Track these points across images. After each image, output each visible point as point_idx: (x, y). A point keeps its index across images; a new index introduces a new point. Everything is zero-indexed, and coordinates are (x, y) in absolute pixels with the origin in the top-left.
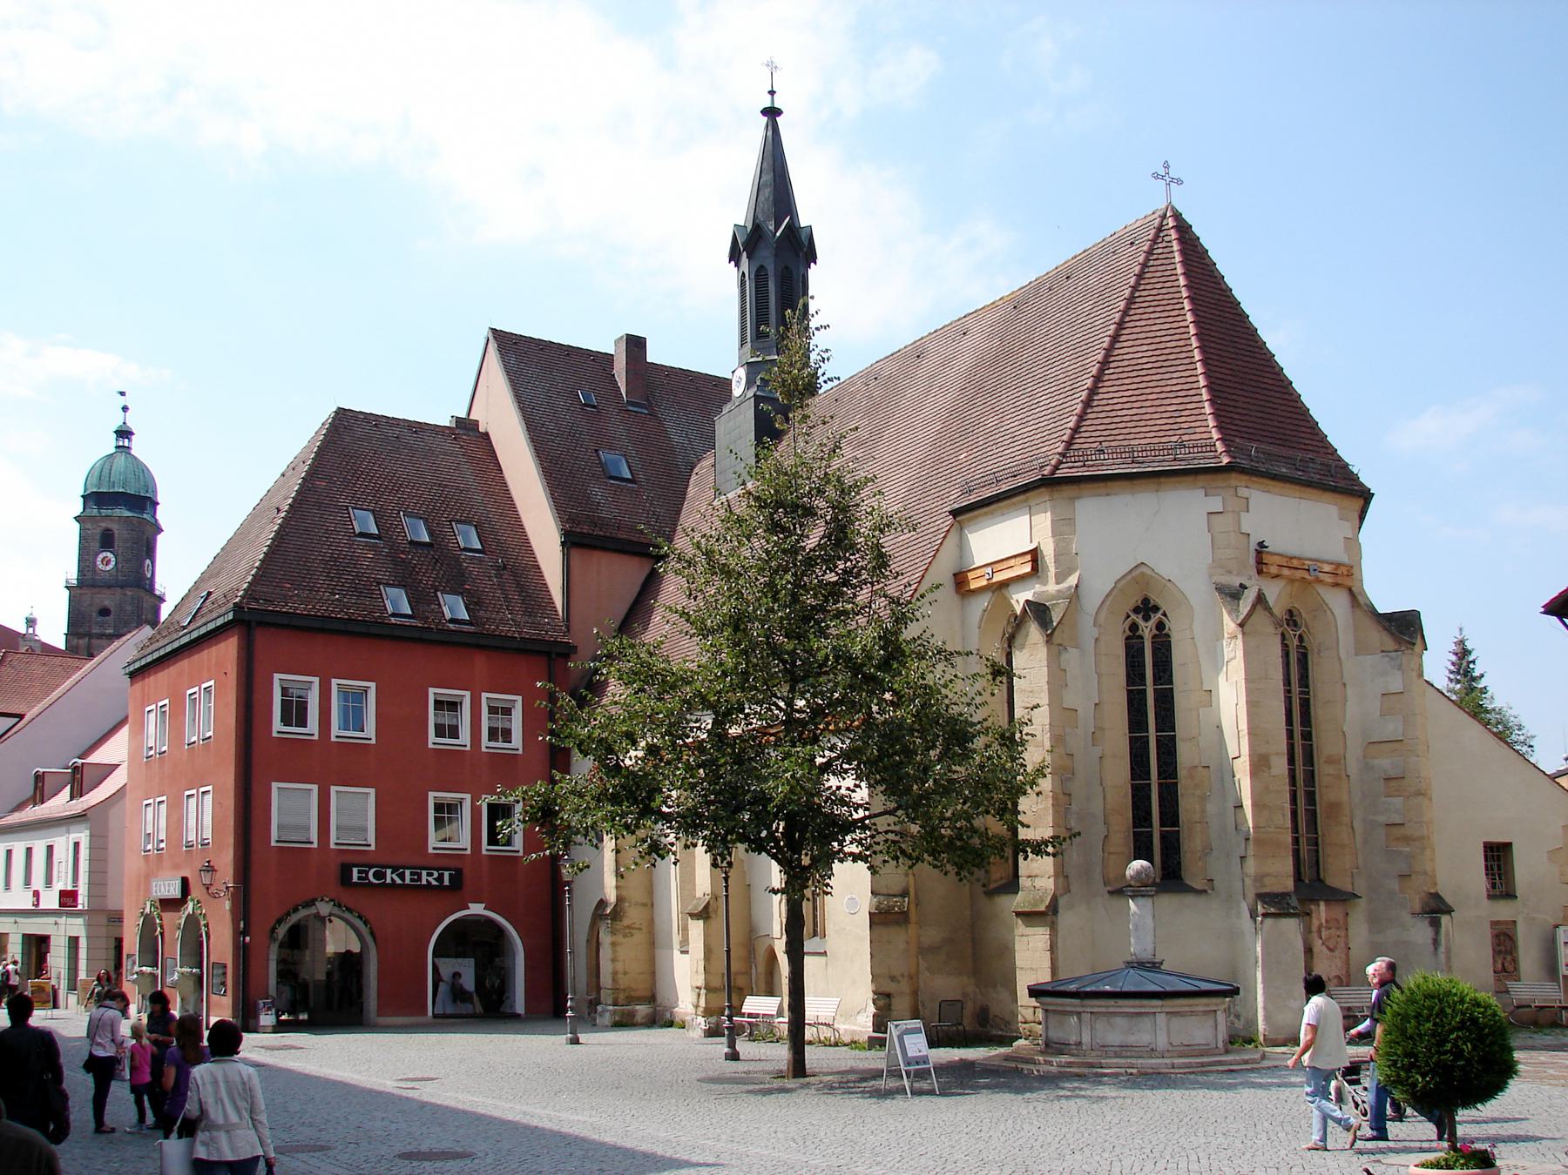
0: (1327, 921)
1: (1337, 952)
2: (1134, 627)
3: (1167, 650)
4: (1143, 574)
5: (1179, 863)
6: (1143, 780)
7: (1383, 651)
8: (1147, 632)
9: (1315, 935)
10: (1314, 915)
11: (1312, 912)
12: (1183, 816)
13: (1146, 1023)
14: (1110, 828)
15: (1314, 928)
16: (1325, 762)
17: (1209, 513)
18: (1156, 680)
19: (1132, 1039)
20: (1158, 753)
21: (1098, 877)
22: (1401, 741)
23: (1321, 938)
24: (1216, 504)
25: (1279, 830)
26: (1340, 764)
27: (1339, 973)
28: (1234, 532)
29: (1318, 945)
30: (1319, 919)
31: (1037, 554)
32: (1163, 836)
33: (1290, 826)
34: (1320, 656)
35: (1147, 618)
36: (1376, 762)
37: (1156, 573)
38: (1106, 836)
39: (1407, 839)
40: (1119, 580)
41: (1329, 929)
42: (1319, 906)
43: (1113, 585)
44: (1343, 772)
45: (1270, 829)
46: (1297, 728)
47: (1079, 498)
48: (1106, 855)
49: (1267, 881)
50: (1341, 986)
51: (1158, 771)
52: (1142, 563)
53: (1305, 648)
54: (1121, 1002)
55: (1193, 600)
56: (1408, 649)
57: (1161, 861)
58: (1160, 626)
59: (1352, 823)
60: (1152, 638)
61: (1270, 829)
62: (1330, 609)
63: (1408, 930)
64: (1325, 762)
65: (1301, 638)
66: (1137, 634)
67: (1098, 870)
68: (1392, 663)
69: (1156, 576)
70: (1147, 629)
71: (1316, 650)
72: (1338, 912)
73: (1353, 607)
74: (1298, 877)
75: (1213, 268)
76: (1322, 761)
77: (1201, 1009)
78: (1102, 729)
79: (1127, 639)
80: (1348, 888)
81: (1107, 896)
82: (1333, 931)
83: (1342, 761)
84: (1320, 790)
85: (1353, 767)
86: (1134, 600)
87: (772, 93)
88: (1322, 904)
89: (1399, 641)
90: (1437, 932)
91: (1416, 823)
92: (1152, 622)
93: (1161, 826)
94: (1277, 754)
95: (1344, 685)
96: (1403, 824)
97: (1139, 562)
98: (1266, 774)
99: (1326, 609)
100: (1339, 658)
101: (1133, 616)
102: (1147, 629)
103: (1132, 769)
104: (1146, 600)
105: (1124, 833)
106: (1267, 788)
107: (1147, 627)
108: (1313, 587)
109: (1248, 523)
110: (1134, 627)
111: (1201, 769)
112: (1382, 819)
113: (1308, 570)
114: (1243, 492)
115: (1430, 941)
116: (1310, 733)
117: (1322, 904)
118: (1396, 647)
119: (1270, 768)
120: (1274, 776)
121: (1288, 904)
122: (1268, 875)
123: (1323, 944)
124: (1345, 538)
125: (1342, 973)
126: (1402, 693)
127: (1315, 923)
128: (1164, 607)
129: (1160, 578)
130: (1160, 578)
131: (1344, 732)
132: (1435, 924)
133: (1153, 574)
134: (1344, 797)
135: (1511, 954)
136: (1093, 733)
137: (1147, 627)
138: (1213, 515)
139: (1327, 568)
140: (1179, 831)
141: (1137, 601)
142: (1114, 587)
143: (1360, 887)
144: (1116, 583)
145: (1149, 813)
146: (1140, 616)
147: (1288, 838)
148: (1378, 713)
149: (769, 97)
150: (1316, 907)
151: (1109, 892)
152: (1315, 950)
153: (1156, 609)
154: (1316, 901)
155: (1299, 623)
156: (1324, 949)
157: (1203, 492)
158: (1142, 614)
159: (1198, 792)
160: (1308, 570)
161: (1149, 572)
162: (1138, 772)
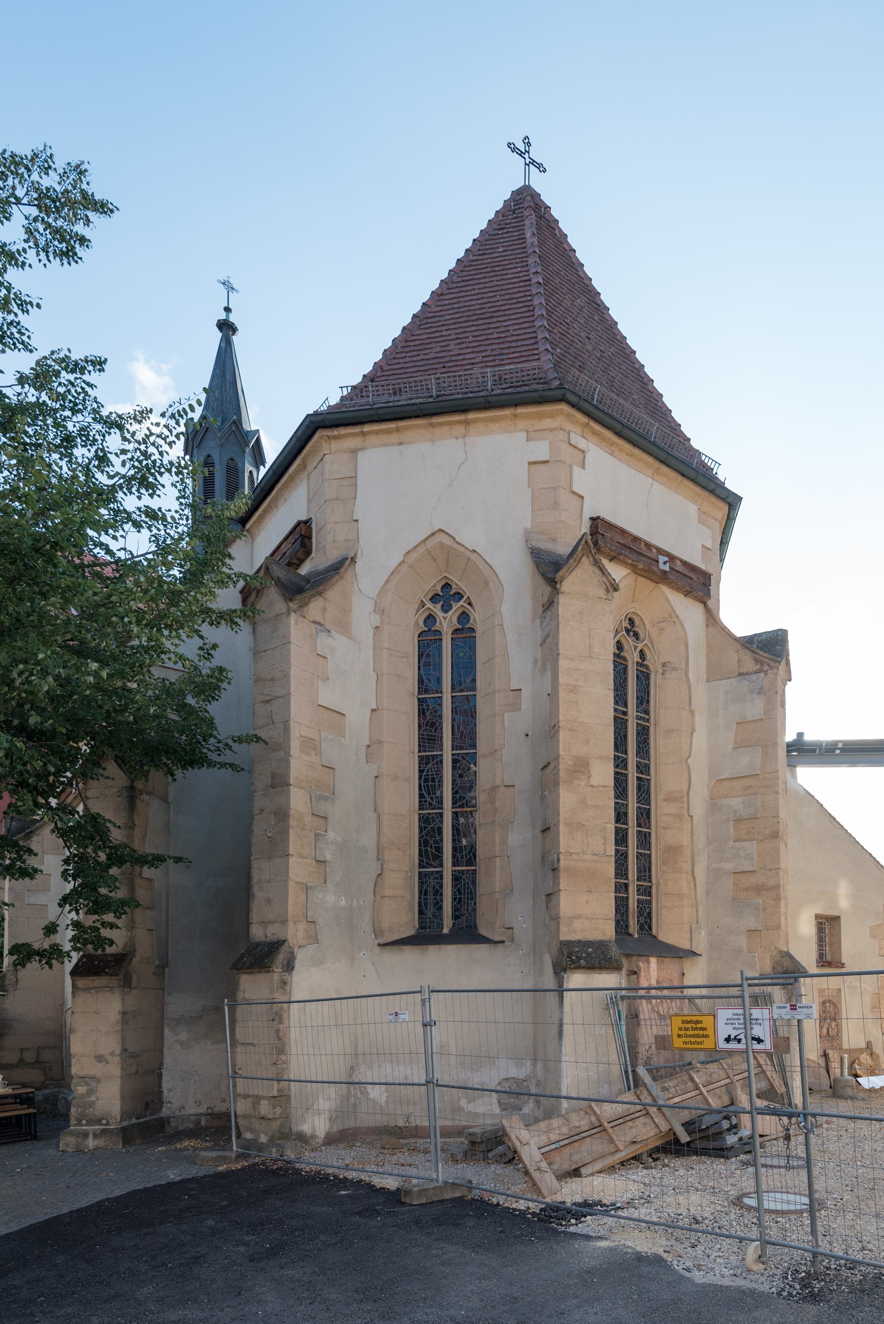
2: (430, 619)
3: (470, 648)
4: (442, 546)
5: (474, 910)
10: (642, 974)
11: (640, 970)
14: (385, 866)
16: (665, 800)
17: (531, 463)
21: (365, 925)
24: (541, 450)
26: (682, 802)
32: (456, 878)
35: (446, 609)
37: (458, 543)
39: (759, 889)
40: (408, 552)
42: (648, 962)
43: (402, 558)
44: (685, 812)
45: (586, 857)
46: (632, 759)
48: (378, 898)
51: (453, 798)
52: (440, 530)
53: (647, 667)
55: (502, 577)
58: (464, 617)
59: (693, 872)
61: (586, 857)
62: (681, 623)
66: (434, 628)
67: (367, 918)
69: (457, 546)
70: (447, 623)
74: (621, 925)
75: (571, 254)
76: (661, 797)
78: (380, 743)
80: (686, 945)
81: (378, 949)
83: (685, 800)
86: (433, 584)
87: (227, 310)
93: (454, 865)
94: (600, 758)
97: (436, 529)
98: (583, 783)
100: (688, 681)
101: (429, 605)
102: (447, 623)
103: (421, 796)
104: (447, 586)
105: (406, 872)
107: (445, 618)
109: (581, 481)
110: (430, 619)
111: (502, 789)
112: (729, 866)
116: (648, 767)
118: (758, 667)
119: (589, 778)
120: (593, 786)
122: (579, 917)
128: (468, 592)
129: (462, 549)
130: (462, 549)
133: (457, 546)
134: (686, 841)
135: (835, 1020)
136: (369, 746)
137: (445, 618)
140: (475, 870)
141: (435, 586)
142: (403, 562)
143: (701, 944)
144: (404, 556)
145: (440, 850)
146: (439, 606)
147: (609, 868)
148: (731, 746)
149: (225, 313)
151: (379, 945)
153: (459, 596)
155: (642, 637)
161: (448, 542)
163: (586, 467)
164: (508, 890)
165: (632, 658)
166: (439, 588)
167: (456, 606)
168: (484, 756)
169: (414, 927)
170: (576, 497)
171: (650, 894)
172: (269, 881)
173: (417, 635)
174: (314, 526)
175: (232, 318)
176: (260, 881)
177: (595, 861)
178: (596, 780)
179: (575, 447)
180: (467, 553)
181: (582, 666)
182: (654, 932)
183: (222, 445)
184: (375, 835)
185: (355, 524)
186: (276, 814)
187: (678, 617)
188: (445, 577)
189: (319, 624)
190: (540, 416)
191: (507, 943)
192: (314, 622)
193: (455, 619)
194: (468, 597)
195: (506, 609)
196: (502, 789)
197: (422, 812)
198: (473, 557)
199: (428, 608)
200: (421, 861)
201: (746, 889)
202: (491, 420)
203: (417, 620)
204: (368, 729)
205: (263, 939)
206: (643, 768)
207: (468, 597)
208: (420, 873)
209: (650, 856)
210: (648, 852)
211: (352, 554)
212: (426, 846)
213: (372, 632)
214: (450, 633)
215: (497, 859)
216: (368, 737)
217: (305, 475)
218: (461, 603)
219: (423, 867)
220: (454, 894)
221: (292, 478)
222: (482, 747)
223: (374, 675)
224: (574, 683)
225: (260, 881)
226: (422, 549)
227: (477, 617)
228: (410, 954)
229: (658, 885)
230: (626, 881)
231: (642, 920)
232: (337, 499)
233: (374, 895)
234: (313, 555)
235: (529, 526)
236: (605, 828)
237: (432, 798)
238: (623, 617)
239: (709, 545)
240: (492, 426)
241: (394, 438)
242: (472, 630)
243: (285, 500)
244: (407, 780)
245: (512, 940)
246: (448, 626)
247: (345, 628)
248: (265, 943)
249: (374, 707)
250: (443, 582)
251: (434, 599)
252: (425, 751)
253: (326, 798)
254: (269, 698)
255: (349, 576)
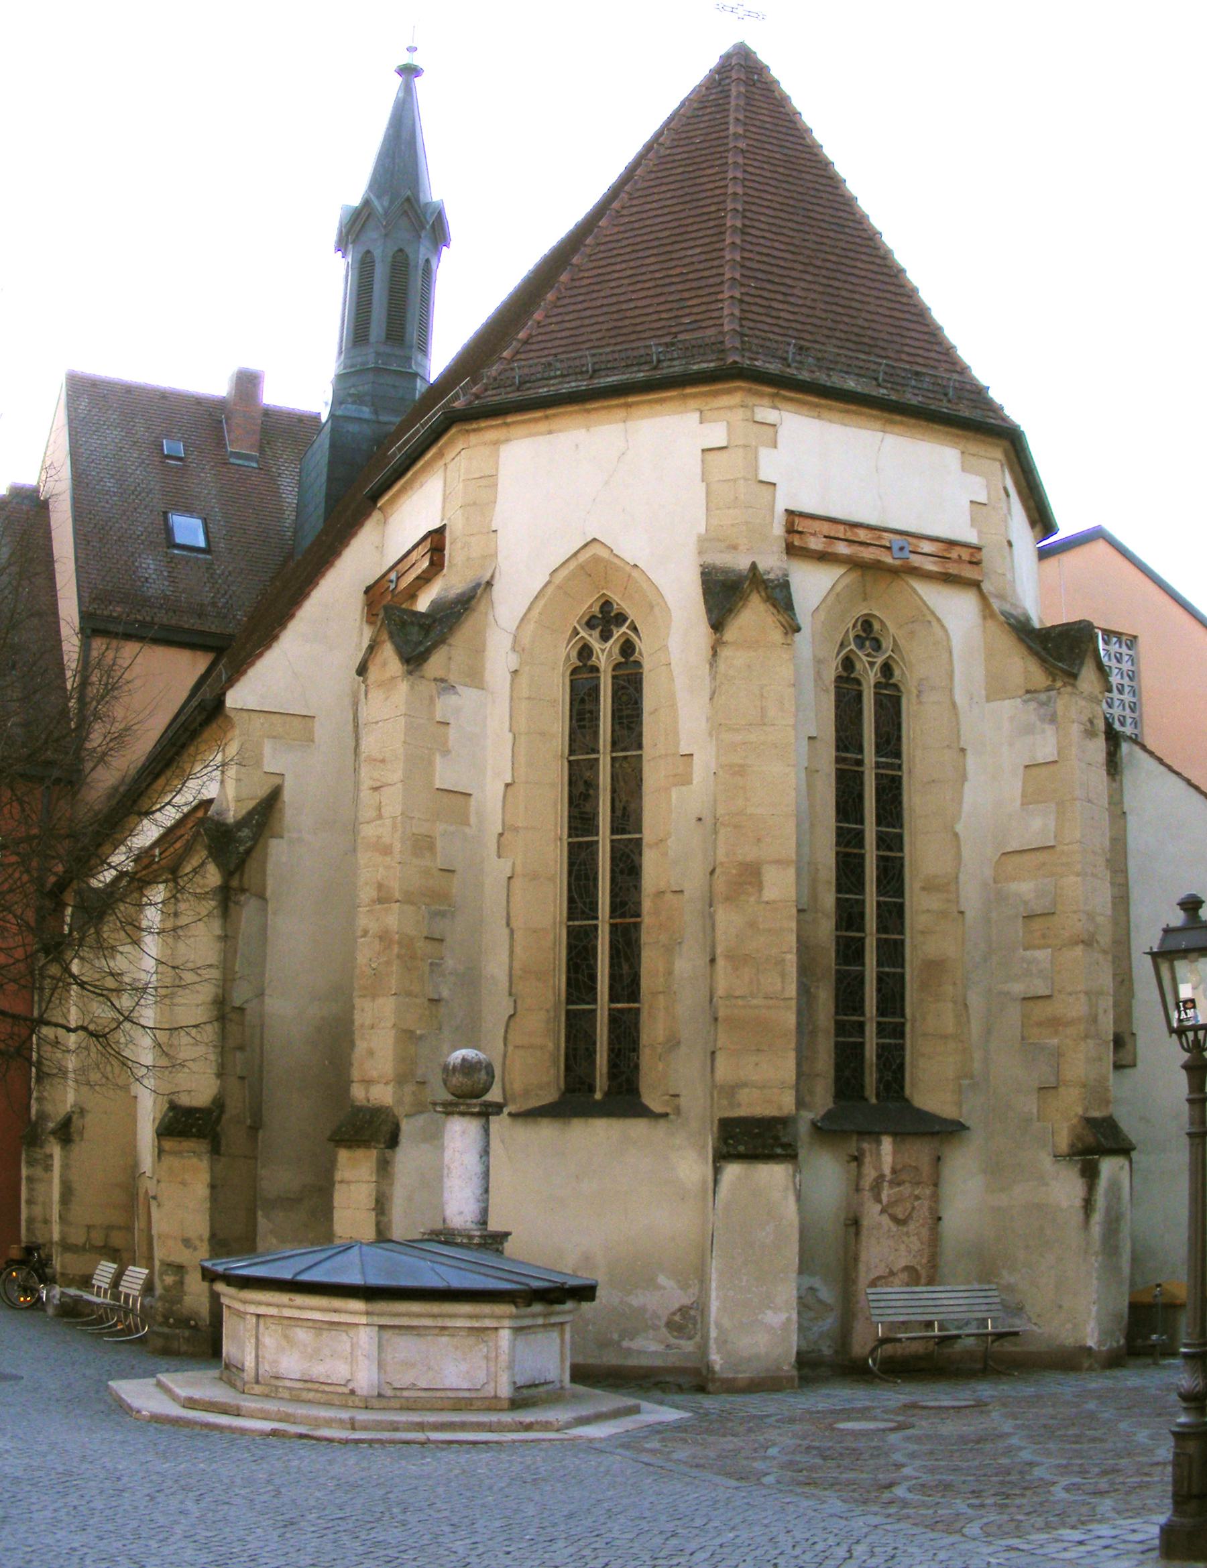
0: (894, 1171)
1: (912, 1226)
2: (585, 652)
4: (596, 559)
6: (588, 919)
7: (1028, 692)
8: (603, 658)
9: (867, 1194)
12: (647, 983)
13: (343, 1341)
14: (519, 1002)
15: (867, 1182)
16: (923, 889)
17: (703, 451)
18: (614, 909)
19: (319, 1370)
20: (612, 871)
22: (1053, 847)
23: (879, 1201)
24: (716, 434)
25: (771, 1002)
27: (913, 1263)
28: (746, 480)
29: (872, 1213)
30: (878, 1167)
31: (444, 538)
33: (794, 994)
34: (920, 703)
35: (605, 637)
36: (1014, 887)
37: (617, 556)
38: (511, 1017)
41: (899, 1184)
43: (547, 578)
45: (755, 1002)
47: (507, 440)
49: (744, 1095)
50: (917, 1285)
51: (612, 903)
52: (595, 540)
54: (300, 1299)
56: (1065, 685)
57: (609, 1062)
58: (628, 648)
60: (614, 670)
61: (755, 1002)
62: (938, 620)
63: (1047, 1185)
64: (923, 889)
65: (887, 669)
66: (590, 663)
68: (1042, 711)
70: (605, 655)
71: (915, 692)
72: (920, 1153)
73: (984, 618)
76: (917, 885)
77: (460, 1323)
79: (574, 672)
82: (906, 1189)
84: (912, 938)
85: (971, 896)
86: (588, 604)
88: (887, 1144)
89: (1052, 673)
90: (1091, 1187)
91: (1070, 994)
92: (613, 645)
93: (612, 999)
95: (963, 750)
96: (1049, 997)
98: (752, 899)
99: (930, 618)
100: (954, 705)
101: (582, 633)
102: (605, 655)
103: (571, 900)
104: (606, 604)
105: (548, 1011)
106: (752, 925)
107: (603, 651)
108: (907, 583)
109: (770, 465)
110: (585, 652)
112: (1018, 988)
113: (889, 548)
114: (766, 413)
115: (1078, 1203)
117: (887, 1144)
118: (1049, 683)
120: (767, 903)
121: (776, 1138)
122: (744, 1085)
123: (882, 1211)
124: (972, 502)
125: (920, 1263)
126: (1056, 762)
127: (870, 1174)
128: (632, 613)
131: (956, 835)
132: (1090, 1174)
137: (603, 651)
138: (712, 454)
139: (927, 547)
141: (591, 606)
142: (549, 583)
143: (970, 1111)
145: (593, 978)
146: (596, 633)
148: (1018, 802)
150: (874, 1146)
152: (865, 1222)
153: (621, 618)
154: (874, 1136)
156: (885, 1220)
157: (696, 415)
158: (600, 628)
159: (663, 938)
160: (889, 548)
161: (605, 554)
162: (580, 905)
163: (779, 445)
164: (673, 1043)
165: (870, 678)
166: (596, 609)
167: (618, 632)
168: (650, 846)
169: (559, 1089)
170: (764, 487)
171: (902, 1035)
172: (372, 1027)
173: (568, 673)
174: (447, 534)
175: (416, 60)
176: (362, 1026)
177: (769, 1008)
178: (769, 894)
179: (762, 423)
180: (628, 568)
181: (752, 737)
182: (908, 1091)
183: (386, 235)
184: (507, 960)
185: (493, 535)
186: (381, 938)
187: (933, 613)
188: (604, 595)
189: (442, 680)
190: (715, 394)
191: (672, 1117)
192: (435, 680)
193: (616, 650)
194: (632, 622)
195: (674, 643)
196: (669, 896)
197: (571, 923)
198: (635, 574)
199: (582, 638)
200: (569, 994)
201: (1039, 1024)
202: (657, 401)
203: (568, 655)
204: (500, 811)
205: (365, 1103)
206: (891, 843)
207: (632, 622)
208: (568, 1012)
209: (902, 976)
210: (899, 970)
211: (487, 577)
212: (576, 972)
213: (509, 677)
214: (610, 669)
215: (661, 997)
216: (500, 822)
217: (442, 463)
218: (624, 629)
219: (573, 1003)
220: (611, 1042)
221: (429, 464)
222: (649, 834)
223: (510, 736)
224: (741, 762)
225: (362, 1026)
226: (572, 565)
227: (645, 647)
228: (547, 1131)
229: (914, 1020)
230: (861, 1019)
231: (889, 1076)
232: (475, 503)
233: (505, 1045)
234: (445, 571)
235: (703, 531)
236: (784, 960)
237: (584, 903)
238: (851, 625)
239: (982, 498)
240: (658, 407)
241: (543, 426)
242: (638, 664)
243: (422, 486)
244: (551, 879)
245: (678, 1111)
246: (607, 659)
247: (475, 678)
248: (368, 1109)
249: (509, 781)
250: (602, 601)
251: (590, 624)
252: (577, 836)
253: (443, 914)
254: (378, 784)
255: (482, 607)
